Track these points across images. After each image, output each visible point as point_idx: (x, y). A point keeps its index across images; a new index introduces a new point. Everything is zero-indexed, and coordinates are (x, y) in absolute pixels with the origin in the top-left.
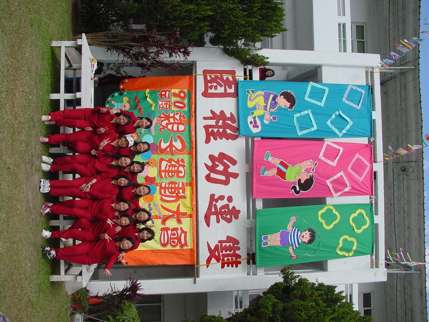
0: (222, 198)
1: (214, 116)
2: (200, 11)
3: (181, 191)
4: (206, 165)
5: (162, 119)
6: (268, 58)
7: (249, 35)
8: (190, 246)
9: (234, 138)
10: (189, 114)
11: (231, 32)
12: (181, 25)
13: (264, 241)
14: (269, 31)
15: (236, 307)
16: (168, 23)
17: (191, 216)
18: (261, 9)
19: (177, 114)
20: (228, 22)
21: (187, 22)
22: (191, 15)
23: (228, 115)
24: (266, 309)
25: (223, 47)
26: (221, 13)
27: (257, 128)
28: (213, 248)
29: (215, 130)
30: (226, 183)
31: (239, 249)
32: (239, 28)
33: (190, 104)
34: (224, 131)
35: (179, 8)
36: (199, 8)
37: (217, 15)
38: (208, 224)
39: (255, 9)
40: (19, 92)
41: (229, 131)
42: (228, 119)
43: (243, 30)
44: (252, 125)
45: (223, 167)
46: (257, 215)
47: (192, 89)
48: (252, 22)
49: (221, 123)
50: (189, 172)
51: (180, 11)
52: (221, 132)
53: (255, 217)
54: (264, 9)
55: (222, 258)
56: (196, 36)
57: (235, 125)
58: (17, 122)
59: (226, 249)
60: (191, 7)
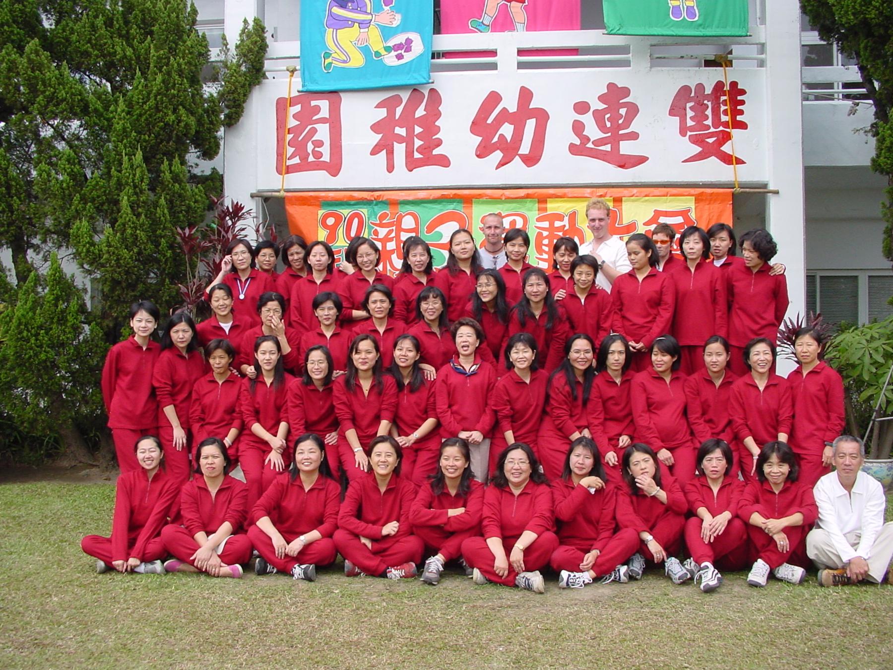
0: (578, 128)
1: (384, 146)
3: (558, 224)
4: (502, 164)
5: (389, 267)
6: (245, 21)
8: (687, 203)
9: (435, 97)
10: (376, 205)
11: (184, 107)
14: (177, 17)
15: (830, 97)
16: (165, 256)
17: (618, 200)
18: (127, 38)
21: (162, 211)
23: (383, 113)
25: (222, 129)
28: (697, 149)
29: (418, 143)
30: (542, 117)
31: (700, 87)
32: (173, 87)
33: (352, 202)
34: (421, 121)
35: (129, 231)
36: (127, 184)
37: (145, 141)
38: (642, 160)
39: (129, 52)
40: (322, 624)
41: (420, 112)
42: (391, 113)
43: (177, 77)
45: (506, 124)
47: (317, 198)
48: (159, 58)
49: (401, 131)
52: (421, 130)
54: (128, 32)
55: (721, 128)
56: (197, 190)
57: (405, 96)
58: (396, 632)
59: (700, 117)
60: (124, 202)
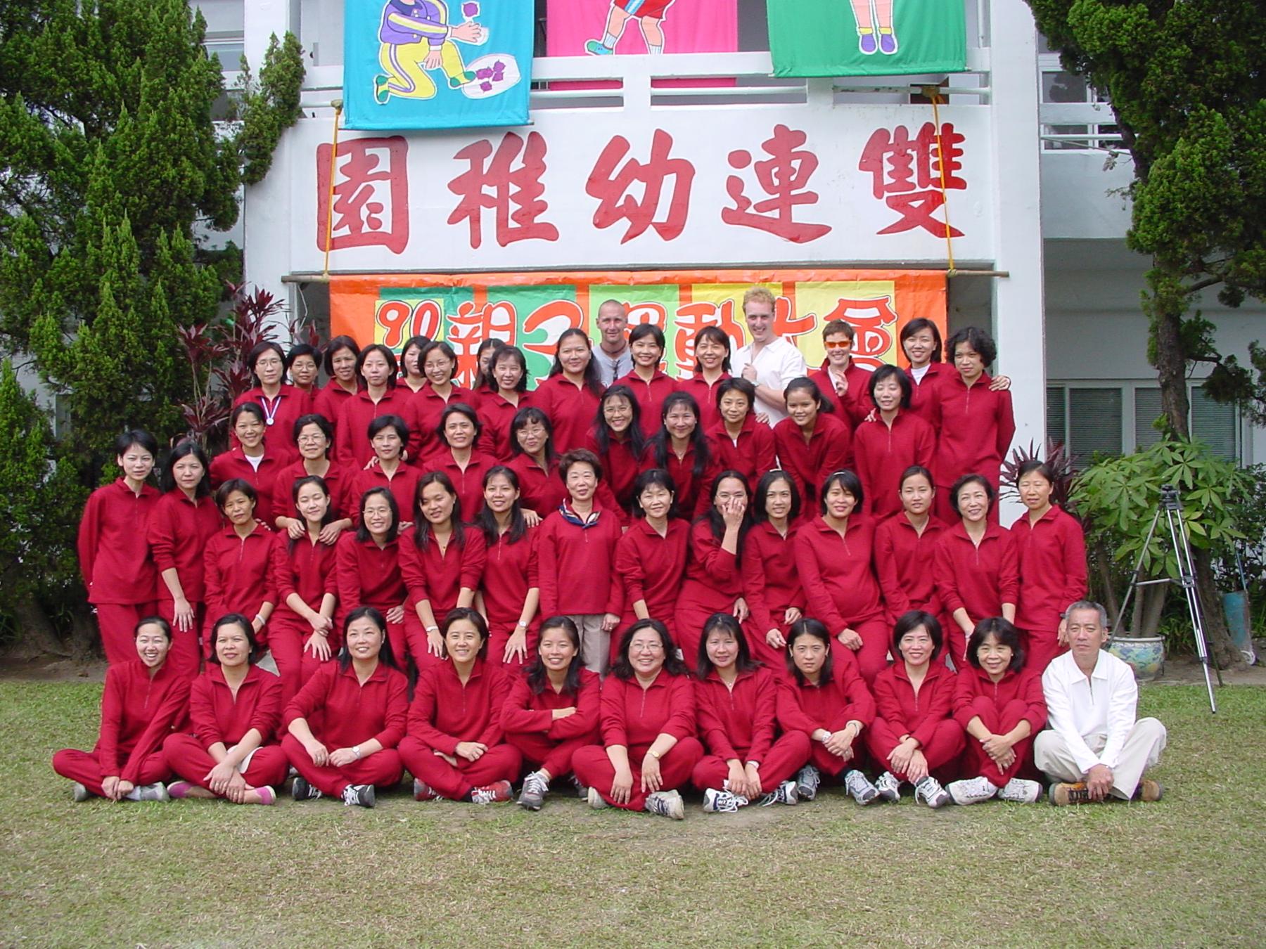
0: (734, 186)
1: (467, 212)
2: (118, 260)
3: (707, 319)
4: (629, 236)
6: (274, 37)
7: (195, 96)
8: (884, 290)
10: (456, 293)
11: (189, 158)
12: (168, 322)
13: (879, 46)
14: (178, 32)
16: (162, 364)
17: (789, 287)
18: (108, 60)
19: (455, 331)
20: (155, 168)
21: (159, 303)
22: (133, 290)
23: (465, 166)
24: (1121, 26)
25: (242, 187)
26: (126, 193)
27: (503, 66)
28: (898, 216)
29: (514, 207)
30: (685, 171)
31: (902, 131)
33: (423, 289)
34: (518, 177)
35: (113, 330)
36: (110, 264)
37: (134, 205)
38: (822, 230)
39: (110, 79)
41: (517, 164)
42: (476, 166)
43: (178, 116)
44: (493, 83)
46: (791, 74)
47: (373, 283)
48: (153, 88)
49: (490, 191)
50: (646, 293)
51: (122, 327)
52: (511, 185)
53: (799, 80)
54: (108, 52)
55: (930, 188)
57: (496, 143)
58: (484, 872)
59: (901, 172)
60: (106, 290)
